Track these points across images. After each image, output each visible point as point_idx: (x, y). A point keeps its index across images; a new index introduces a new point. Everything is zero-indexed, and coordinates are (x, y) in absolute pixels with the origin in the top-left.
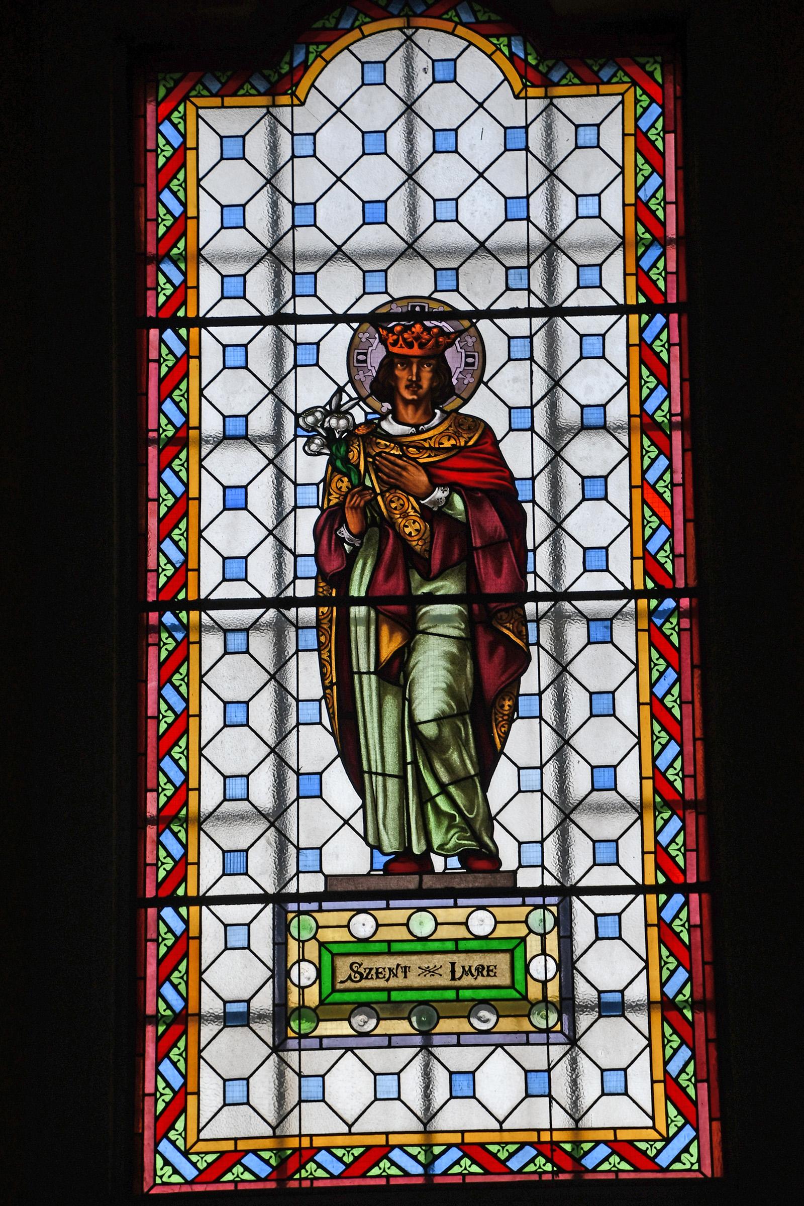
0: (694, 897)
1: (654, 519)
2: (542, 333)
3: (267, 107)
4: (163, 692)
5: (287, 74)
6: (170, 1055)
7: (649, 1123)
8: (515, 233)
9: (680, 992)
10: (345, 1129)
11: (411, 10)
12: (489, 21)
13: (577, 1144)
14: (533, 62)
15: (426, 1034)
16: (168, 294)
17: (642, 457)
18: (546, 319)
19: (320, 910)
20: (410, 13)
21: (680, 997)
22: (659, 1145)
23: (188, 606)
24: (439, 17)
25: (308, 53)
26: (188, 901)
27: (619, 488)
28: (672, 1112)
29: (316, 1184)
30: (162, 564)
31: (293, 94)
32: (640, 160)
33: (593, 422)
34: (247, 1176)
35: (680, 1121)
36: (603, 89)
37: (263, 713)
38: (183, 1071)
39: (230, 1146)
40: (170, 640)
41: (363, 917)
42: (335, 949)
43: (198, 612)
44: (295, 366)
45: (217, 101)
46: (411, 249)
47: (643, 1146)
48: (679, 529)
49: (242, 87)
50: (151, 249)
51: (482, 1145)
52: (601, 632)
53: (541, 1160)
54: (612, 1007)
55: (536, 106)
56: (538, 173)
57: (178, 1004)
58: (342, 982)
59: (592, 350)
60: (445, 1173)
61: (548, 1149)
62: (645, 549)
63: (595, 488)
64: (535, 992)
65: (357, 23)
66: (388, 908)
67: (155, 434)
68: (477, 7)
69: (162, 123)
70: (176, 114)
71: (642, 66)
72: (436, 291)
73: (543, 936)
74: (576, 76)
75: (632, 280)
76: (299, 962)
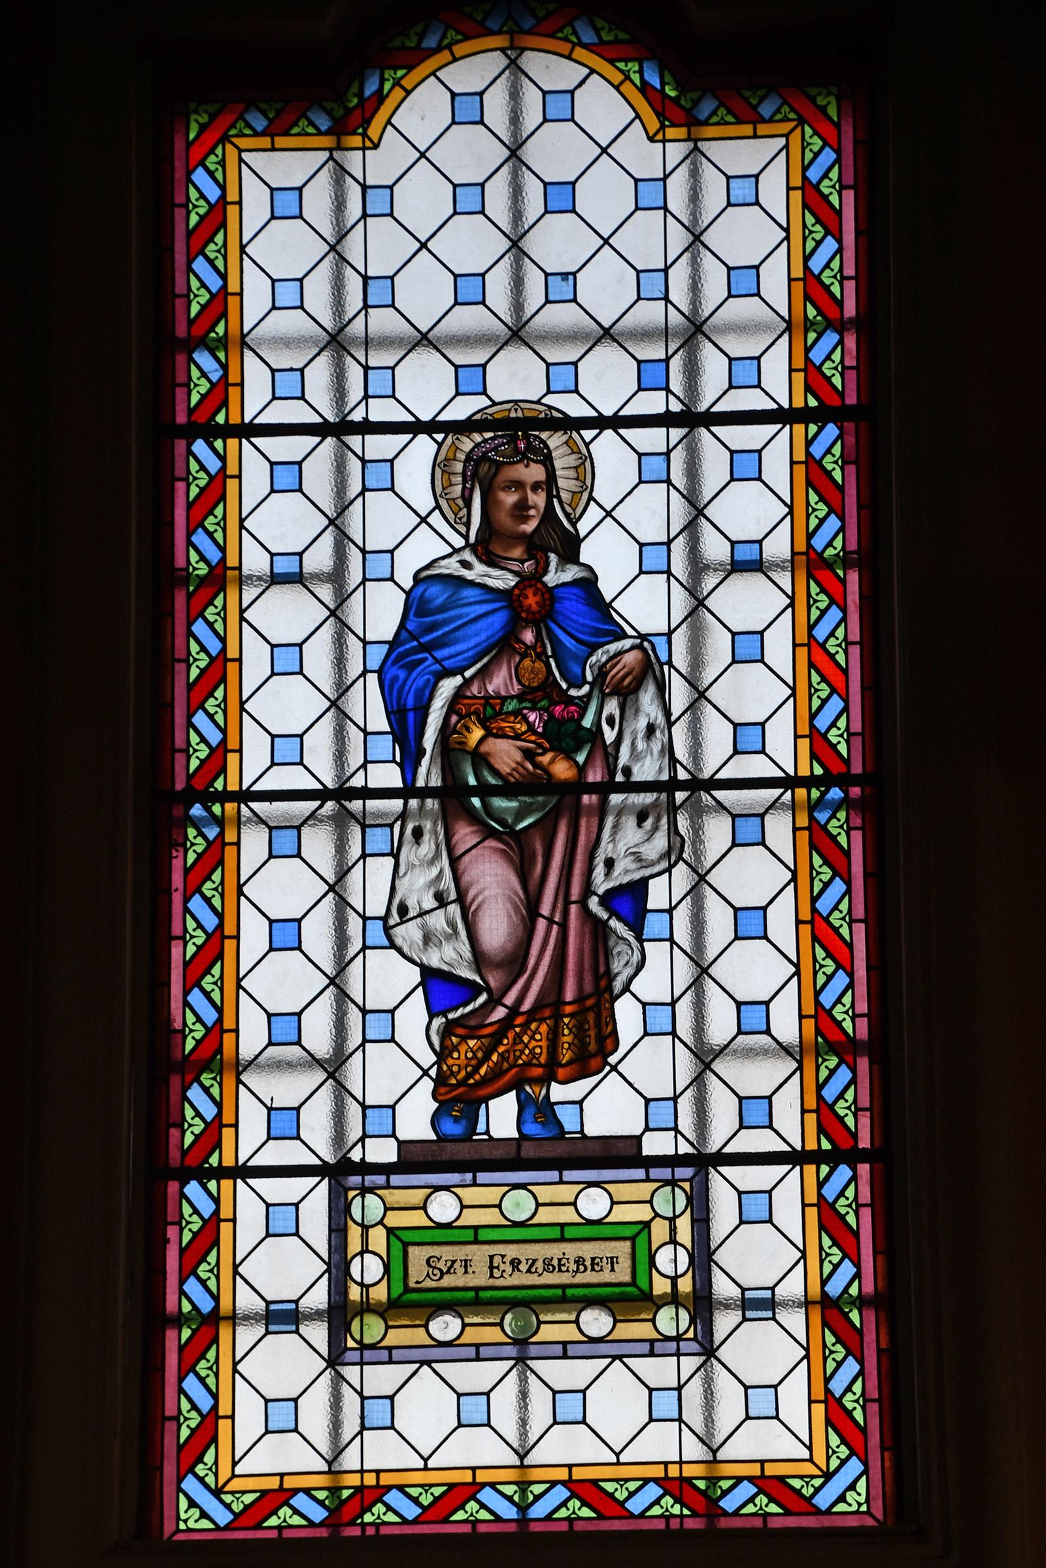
0: (850, 426)
1: (823, 686)
2: (688, 997)
3: (330, 150)
4: (185, 1385)
5: (356, 107)
6: (204, 1031)
7: (805, 1454)
8: (651, 313)
9: (830, 544)
10: (420, 1464)
11: (516, 23)
12: (616, 42)
13: (713, 1480)
14: (673, 94)
15: (521, 1343)
16: (197, 1132)
17: (815, 973)
18: (687, 430)
19: (388, 1186)
20: (515, 28)
21: (830, 552)
22: (817, 1482)
23: (225, 797)
24: (552, 35)
25: (382, 81)
26: (221, 1173)
27: (779, 647)
28: (834, 1440)
29: (384, 1531)
30: (189, 1023)
31: (365, 135)
32: (810, 220)
33: (747, 562)
34: (297, 1520)
35: (844, 1451)
36: (762, 129)
37: (318, 935)
38: (221, 543)
39: (274, 1483)
40: (200, 840)
41: (443, 1196)
42: (407, 1236)
43: (237, 440)
44: (364, 856)
45: (266, 142)
46: (517, 333)
47: (796, 1483)
48: (853, 593)
49: (296, 124)
50: (181, 331)
51: (595, 1482)
52: (748, 832)
53: (668, 1501)
54: (759, 1305)
55: (676, 151)
56: (678, 238)
57: (206, 1305)
58: (417, 1282)
59: (745, 468)
60: (549, 1517)
61: (675, 1485)
62: (806, 268)
63: (748, 648)
64: (661, 1286)
65: (446, 42)
66: (474, 1184)
67: (184, 573)
68: (600, 23)
69: (189, 1087)
70: (212, 158)
71: (813, 100)
72: (549, 392)
73: (672, 1220)
74: (730, 112)
75: (804, 744)
76: (361, 1253)
